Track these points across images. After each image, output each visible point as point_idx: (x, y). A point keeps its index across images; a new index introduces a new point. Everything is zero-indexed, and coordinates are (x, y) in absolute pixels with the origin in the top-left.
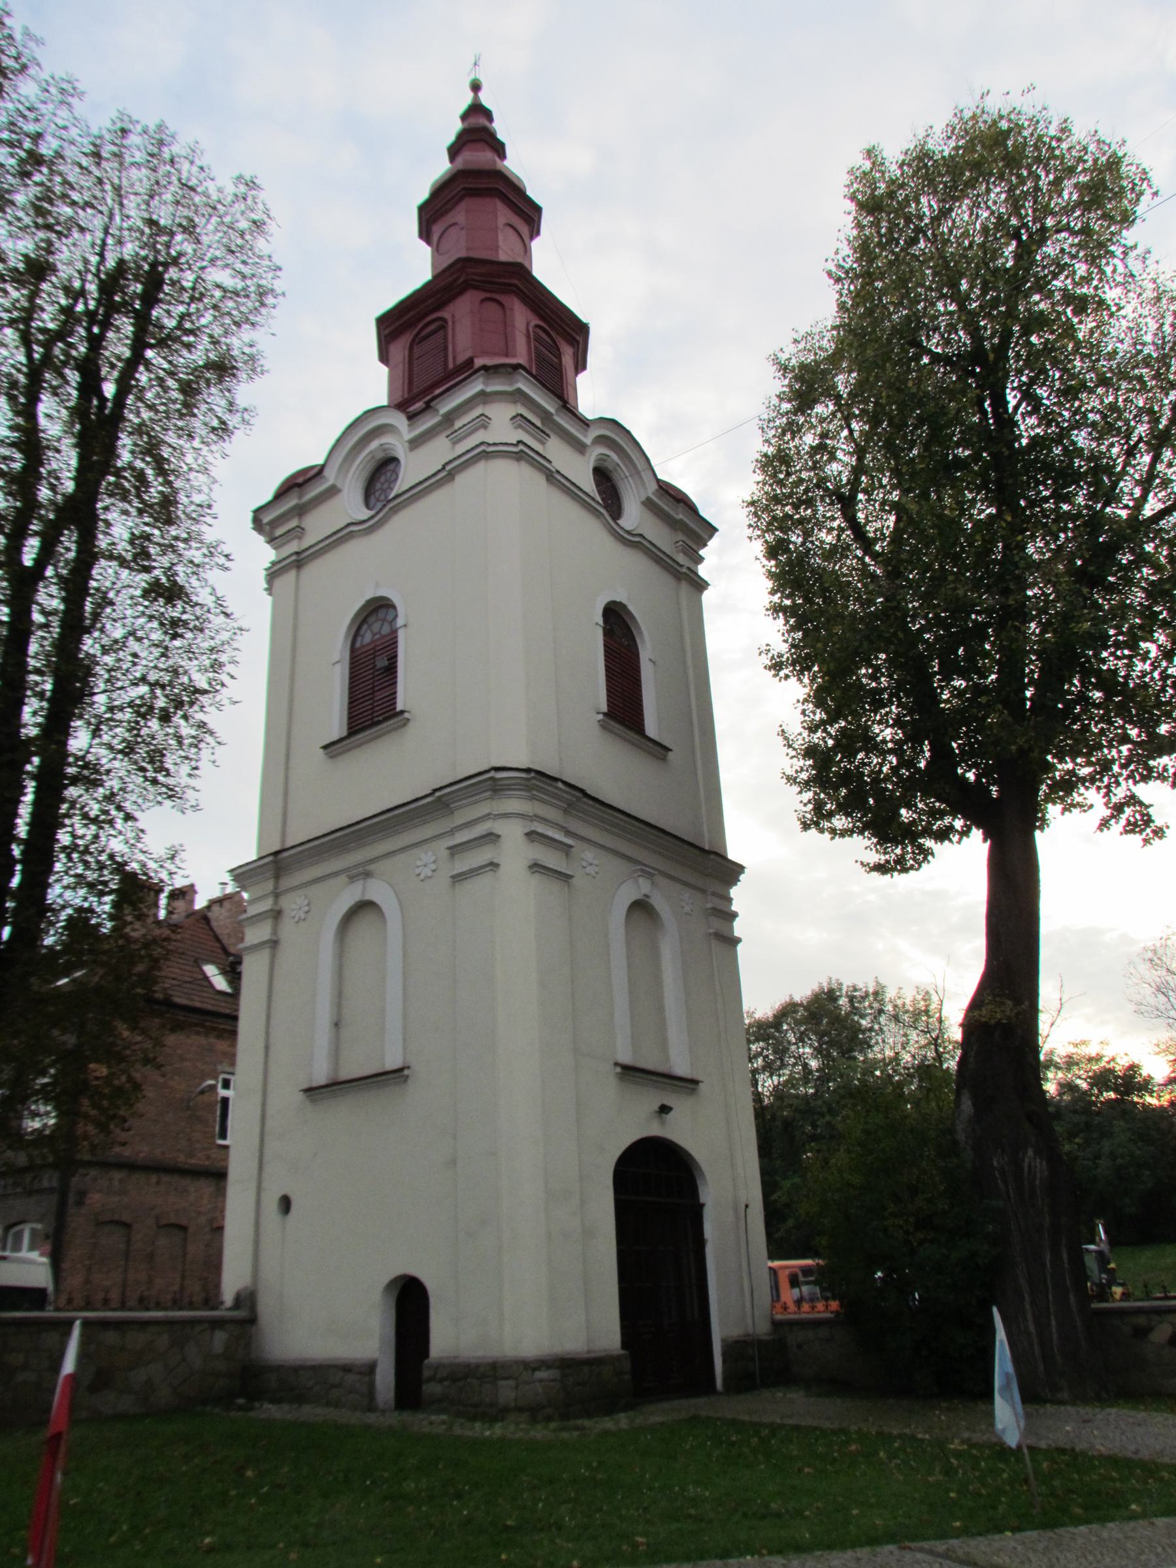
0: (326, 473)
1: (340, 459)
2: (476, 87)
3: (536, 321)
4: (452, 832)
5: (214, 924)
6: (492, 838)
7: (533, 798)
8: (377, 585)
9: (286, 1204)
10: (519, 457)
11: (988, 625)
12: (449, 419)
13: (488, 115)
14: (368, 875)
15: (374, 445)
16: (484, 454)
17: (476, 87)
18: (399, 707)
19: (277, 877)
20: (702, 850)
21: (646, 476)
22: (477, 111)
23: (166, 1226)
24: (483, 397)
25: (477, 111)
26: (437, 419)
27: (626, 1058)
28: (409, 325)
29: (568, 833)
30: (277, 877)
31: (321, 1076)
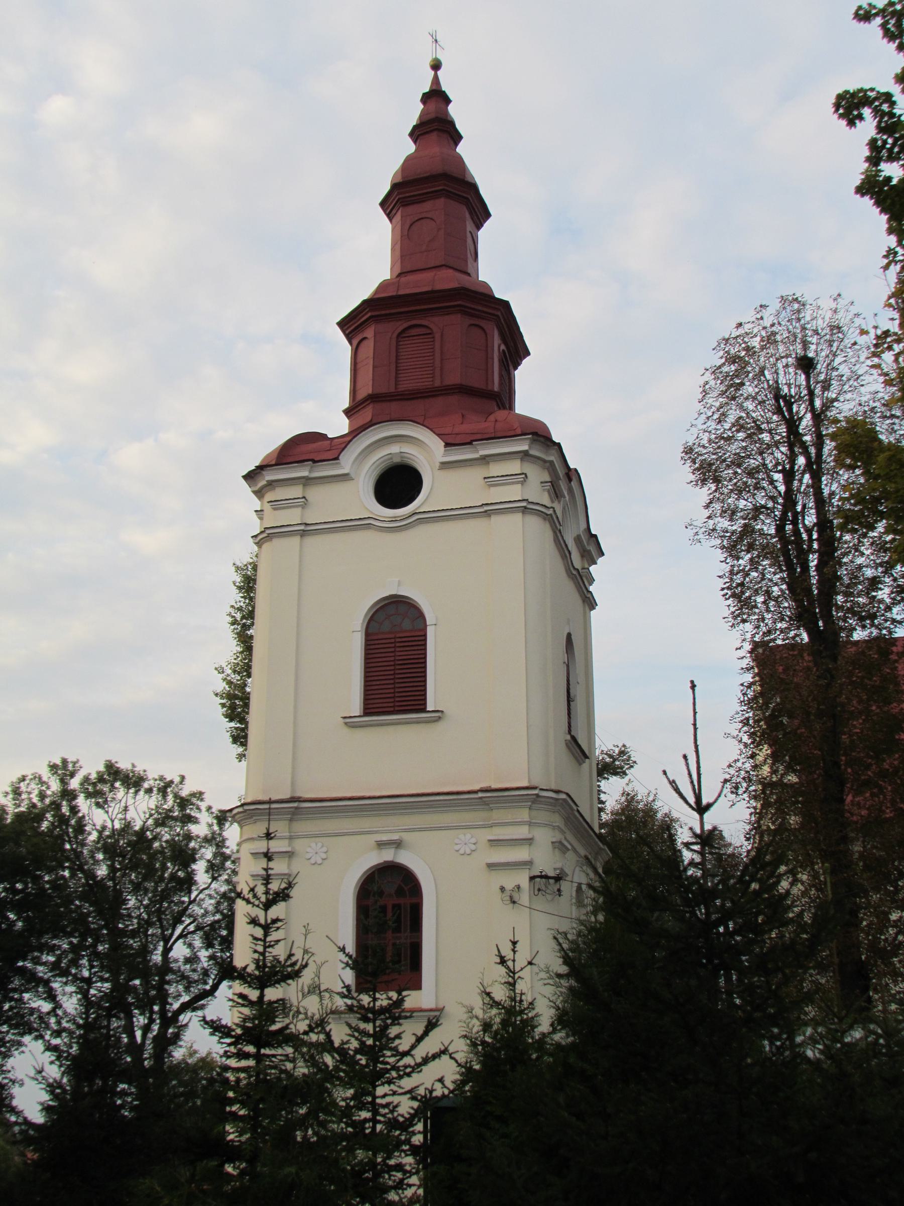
2: (436, 66)
15: (395, 449)
17: (436, 66)
22: (436, 97)
25: (436, 97)
26: (476, 456)
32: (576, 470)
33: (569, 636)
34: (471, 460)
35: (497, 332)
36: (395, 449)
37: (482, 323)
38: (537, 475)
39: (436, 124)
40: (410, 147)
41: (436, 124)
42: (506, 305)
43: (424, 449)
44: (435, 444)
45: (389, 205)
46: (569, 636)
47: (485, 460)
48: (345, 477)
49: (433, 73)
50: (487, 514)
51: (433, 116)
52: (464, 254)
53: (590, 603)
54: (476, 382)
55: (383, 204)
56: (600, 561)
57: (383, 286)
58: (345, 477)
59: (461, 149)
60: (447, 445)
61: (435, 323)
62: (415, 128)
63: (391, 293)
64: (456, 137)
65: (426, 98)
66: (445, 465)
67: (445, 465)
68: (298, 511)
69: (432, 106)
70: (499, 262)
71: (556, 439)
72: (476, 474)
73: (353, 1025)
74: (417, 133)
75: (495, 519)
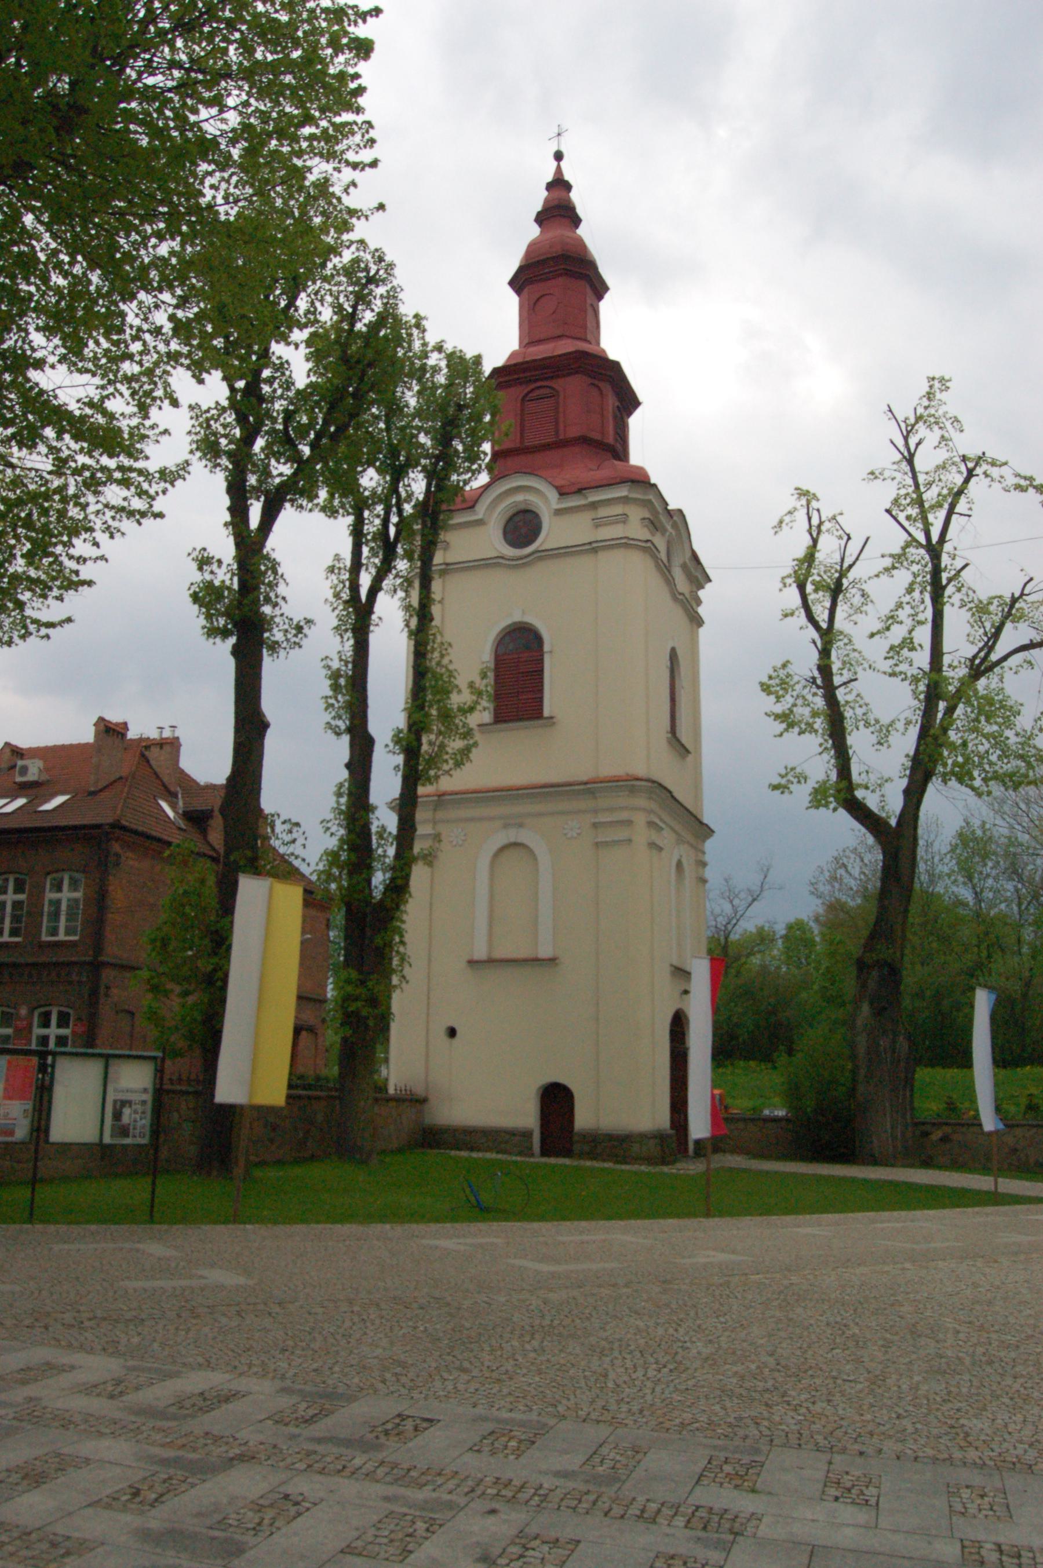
0: (478, 508)
1: (489, 500)
2: (559, 156)
3: (617, 404)
4: (595, 811)
5: (152, 762)
6: (629, 823)
7: (650, 798)
8: (524, 613)
9: (452, 1032)
10: (645, 550)
11: (294, 218)
12: (594, 506)
13: (568, 187)
14: (521, 825)
15: (520, 497)
16: (626, 544)
17: (559, 156)
18: (546, 713)
19: (435, 810)
20: (701, 823)
21: (687, 545)
22: (559, 185)
23: (122, 1011)
24: (625, 500)
25: (559, 185)
26: (583, 502)
27: (675, 963)
28: (518, 382)
29: (661, 820)
30: (435, 810)
31: (481, 952)
32: (680, 511)
33: (673, 651)
34: (613, 499)
35: (613, 391)
36: (520, 497)
37: (601, 385)
38: (636, 514)
39: (559, 209)
40: (535, 231)
41: (559, 209)
42: (616, 366)
43: (542, 496)
44: (552, 495)
45: (518, 283)
46: (673, 651)
47: (594, 506)
48: (480, 523)
49: (555, 164)
50: (595, 551)
51: (556, 203)
52: (587, 323)
53: (697, 621)
54: (596, 436)
55: (512, 283)
56: (708, 586)
57: (513, 355)
58: (480, 523)
59: (581, 231)
60: (561, 494)
61: (558, 384)
62: (539, 214)
63: (520, 360)
64: (576, 221)
65: (550, 186)
66: (558, 512)
67: (558, 512)
68: (620, 527)
69: (558, 193)
70: (622, 331)
71: (653, 481)
72: (584, 519)
73: (878, 626)
74: (541, 219)
75: (602, 556)
